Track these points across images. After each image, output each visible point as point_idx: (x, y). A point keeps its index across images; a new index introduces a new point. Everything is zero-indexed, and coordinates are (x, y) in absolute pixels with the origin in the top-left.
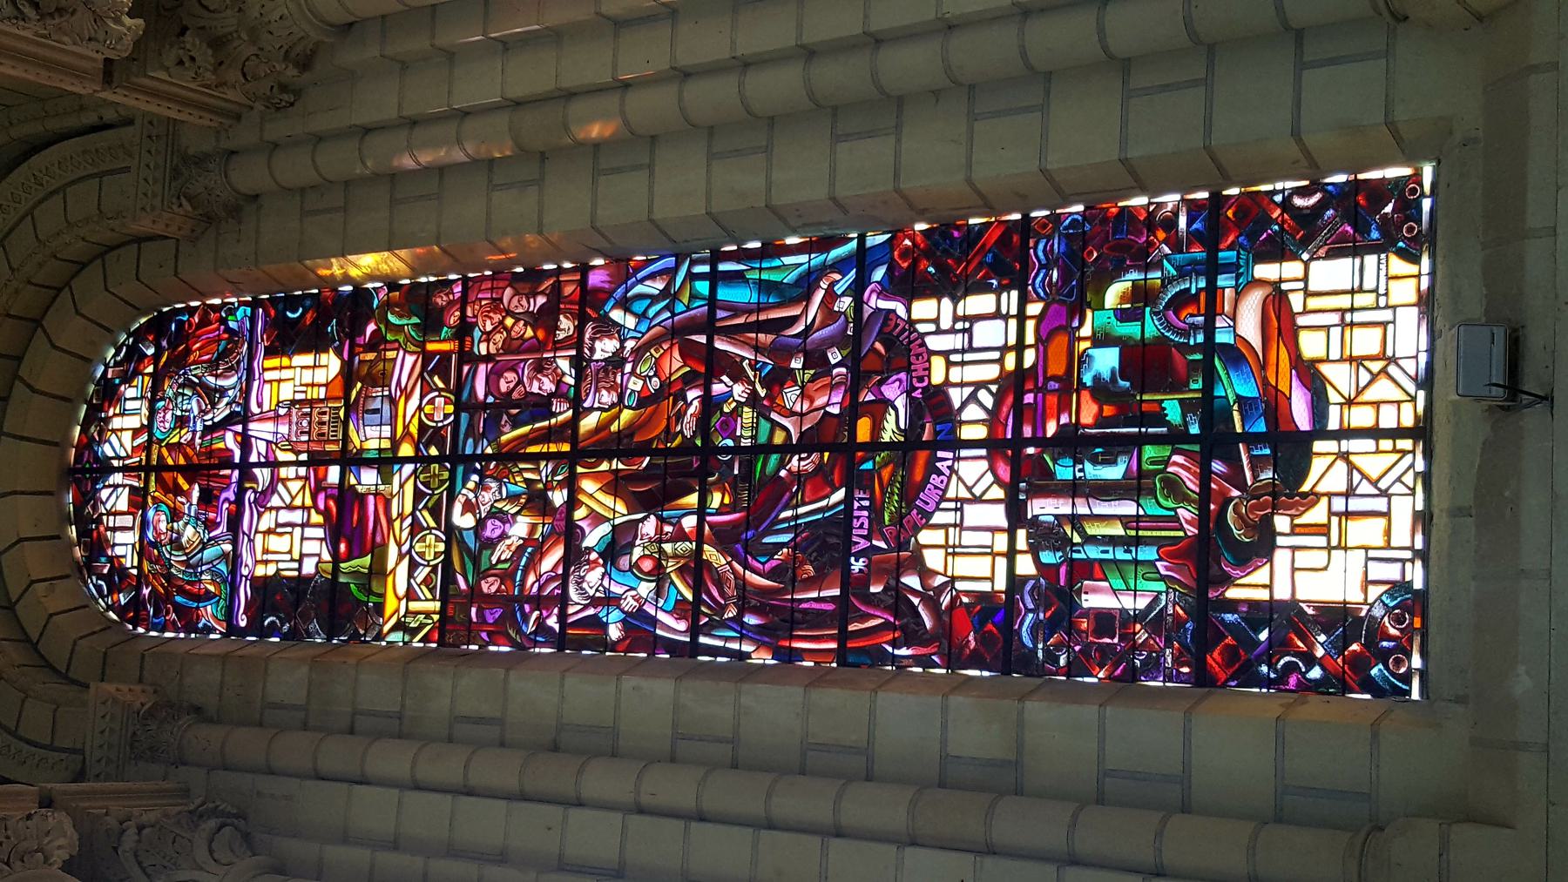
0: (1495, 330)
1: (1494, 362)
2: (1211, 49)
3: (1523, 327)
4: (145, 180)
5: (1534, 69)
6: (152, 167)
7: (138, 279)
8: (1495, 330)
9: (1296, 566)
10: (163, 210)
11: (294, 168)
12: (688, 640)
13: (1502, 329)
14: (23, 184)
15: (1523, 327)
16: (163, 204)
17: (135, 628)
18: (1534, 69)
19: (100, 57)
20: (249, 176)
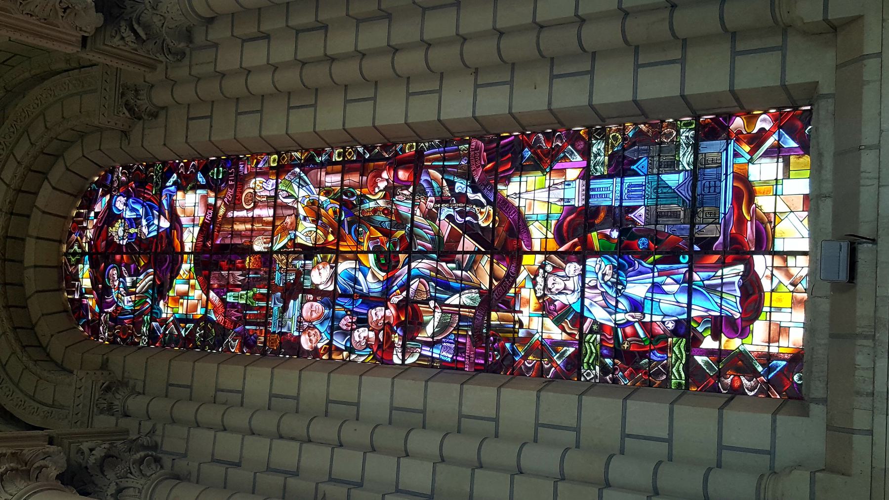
0: (842, 243)
1: (841, 264)
2: (685, 43)
3: (433, 412)
4: (106, 73)
5: (869, 56)
6: (108, 90)
7: (66, 347)
8: (842, 243)
9: (627, 431)
10: (114, 115)
11: (185, 93)
12: (684, 340)
13: (846, 243)
14: (34, 408)
15: (433, 412)
16: (114, 112)
17: (184, 163)
18: (869, 56)
19: (79, 35)
20: (161, 97)
